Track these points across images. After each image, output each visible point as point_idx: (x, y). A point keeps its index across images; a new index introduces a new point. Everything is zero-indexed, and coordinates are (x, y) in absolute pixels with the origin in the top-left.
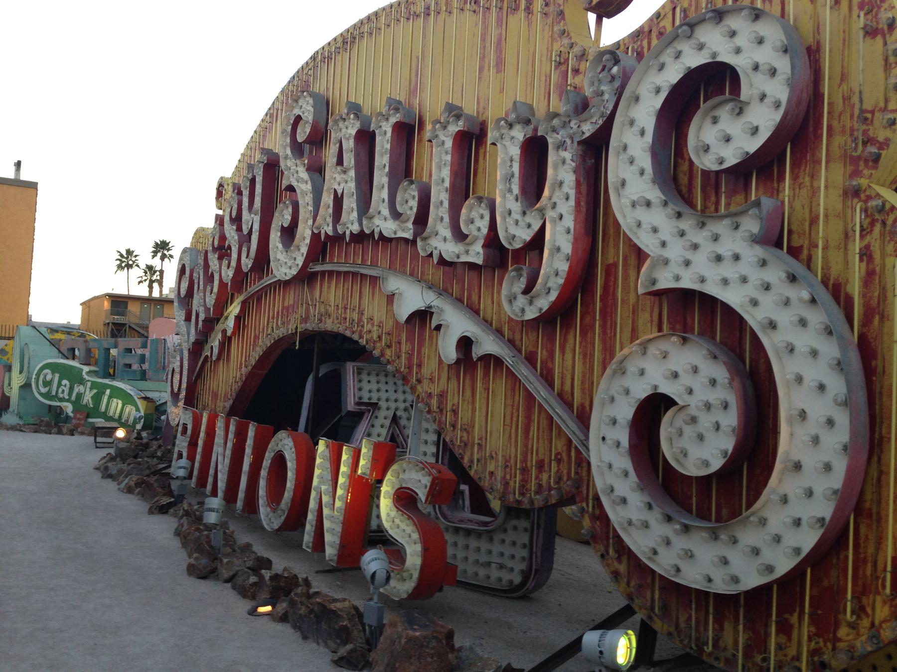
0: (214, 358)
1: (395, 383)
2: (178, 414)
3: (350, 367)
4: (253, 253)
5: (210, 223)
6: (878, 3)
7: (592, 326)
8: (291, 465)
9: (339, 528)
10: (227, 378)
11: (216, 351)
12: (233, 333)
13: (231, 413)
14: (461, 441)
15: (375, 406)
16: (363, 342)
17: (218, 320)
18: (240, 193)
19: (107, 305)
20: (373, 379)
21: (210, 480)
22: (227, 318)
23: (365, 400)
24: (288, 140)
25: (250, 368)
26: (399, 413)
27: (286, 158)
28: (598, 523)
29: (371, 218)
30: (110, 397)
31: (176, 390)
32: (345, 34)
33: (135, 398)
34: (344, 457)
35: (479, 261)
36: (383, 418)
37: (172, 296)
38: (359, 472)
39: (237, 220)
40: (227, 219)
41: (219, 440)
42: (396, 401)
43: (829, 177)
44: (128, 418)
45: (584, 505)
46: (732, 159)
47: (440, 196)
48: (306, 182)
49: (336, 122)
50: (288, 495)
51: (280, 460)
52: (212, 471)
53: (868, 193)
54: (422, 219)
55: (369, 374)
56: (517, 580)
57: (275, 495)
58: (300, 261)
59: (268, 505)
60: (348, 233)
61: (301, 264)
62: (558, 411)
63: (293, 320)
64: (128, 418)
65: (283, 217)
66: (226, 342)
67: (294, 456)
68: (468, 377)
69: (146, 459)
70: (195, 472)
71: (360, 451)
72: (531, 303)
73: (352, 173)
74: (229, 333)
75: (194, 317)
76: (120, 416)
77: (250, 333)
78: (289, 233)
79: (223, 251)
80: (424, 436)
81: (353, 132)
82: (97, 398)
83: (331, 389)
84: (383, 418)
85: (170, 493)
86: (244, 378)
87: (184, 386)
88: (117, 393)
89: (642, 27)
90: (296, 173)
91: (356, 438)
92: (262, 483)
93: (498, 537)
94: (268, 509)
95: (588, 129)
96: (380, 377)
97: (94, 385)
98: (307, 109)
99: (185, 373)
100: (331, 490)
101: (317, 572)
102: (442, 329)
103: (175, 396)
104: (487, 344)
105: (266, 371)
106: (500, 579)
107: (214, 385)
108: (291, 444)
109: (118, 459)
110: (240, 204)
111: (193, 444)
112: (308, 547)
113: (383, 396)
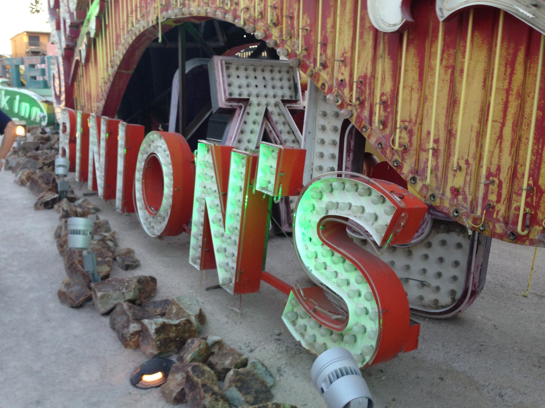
1: (264, 78)
2: (61, 115)
3: (218, 61)
8: (167, 169)
10: (98, 80)
11: (84, 54)
12: (97, 34)
13: (106, 111)
14: (400, 145)
15: (246, 101)
16: (239, 23)
19: (26, 39)
20: (242, 73)
21: (90, 176)
22: (89, 21)
23: (236, 96)
25: (116, 68)
26: (270, 109)
30: (20, 101)
31: (58, 93)
33: (39, 102)
36: (255, 113)
41: (93, 138)
42: (266, 96)
44: (36, 117)
51: (153, 163)
52: (90, 168)
55: (237, 69)
56: (445, 300)
57: (154, 198)
59: (146, 208)
63: (152, 10)
64: (36, 117)
66: (92, 44)
67: (169, 159)
68: (413, 51)
69: (45, 151)
74: (92, 35)
75: (62, 25)
76: (30, 116)
77: (111, 33)
80: (320, 135)
82: (11, 103)
83: (199, 88)
84: (255, 113)
85: (54, 188)
86: (112, 79)
87: (63, 89)
88: (25, 98)
91: (230, 135)
92: (138, 185)
93: (418, 253)
96: (248, 72)
97: (7, 93)
99: (62, 77)
100: (217, 202)
101: (208, 289)
103: (58, 97)
105: (131, 72)
106: (421, 298)
108: (165, 146)
109: (20, 153)
111: (72, 141)
112: (195, 263)
113: (254, 91)
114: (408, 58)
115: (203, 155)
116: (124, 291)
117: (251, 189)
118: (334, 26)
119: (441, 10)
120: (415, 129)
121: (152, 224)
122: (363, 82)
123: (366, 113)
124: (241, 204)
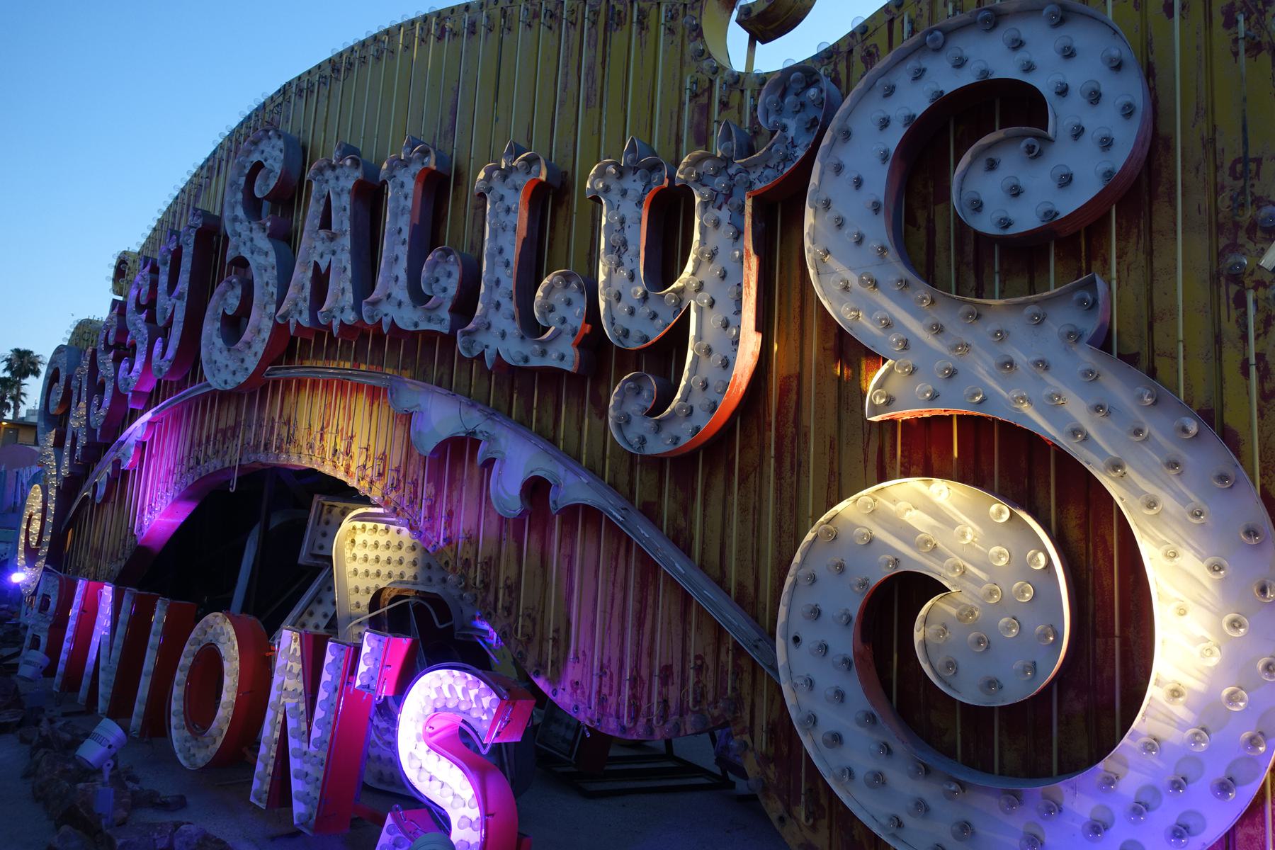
0: (98, 500)
4: (170, 353)
5: (101, 311)
6: (1260, 6)
7: (759, 467)
9: (318, 773)
11: (102, 490)
17: (107, 447)
18: (155, 270)
24: (240, 196)
27: (235, 219)
28: (772, 766)
29: (375, 303)
32: (337, 60)
34: (329, 658)
35: (570, 365)
37: (34, 419)
38: (358, 683)
39: (148, 307)
40: (131, 305)
43: (1184, 257)
45: (747, 737)
46: (1026, 219)
47: (499, 276)
48: (266, 254)
49: (320, 171)
50: (225, 711)
51: (210, 660)
53: (1256, 277)
54: (465, 305)
58: (252, 364)
60: (336, 323)
61: (252, 369)
62: (706, 593)
65: (226, 299)
68: (535, 536)
70: (61, 668)
71: (358, 649)
72: (659, 427)
73: (346, 241)
78: (234, 326)
79: (122, 349)
81: (350, 184)
87: (47, 539)
89: (836, 46)
90: (251, 242)
92: (178, 691)
94: (187, 733)
95: (763, 181)
98: (273, 156)
100: (302, 707)
101: (273, 839)
102: (496, 466)
104: (574, 488)
107: (95, 539)
110: (154, 285)
112: (259, 800)
114: (530, 543)
115: (289, 643)
116: (156, 836)
117: (348, 690)
118: (460, 501)
119: (555, 502)
120: (538, 617)
121: (192, 751)
122: (488, 563)
123: (491, 598)
124: (333, 709)
